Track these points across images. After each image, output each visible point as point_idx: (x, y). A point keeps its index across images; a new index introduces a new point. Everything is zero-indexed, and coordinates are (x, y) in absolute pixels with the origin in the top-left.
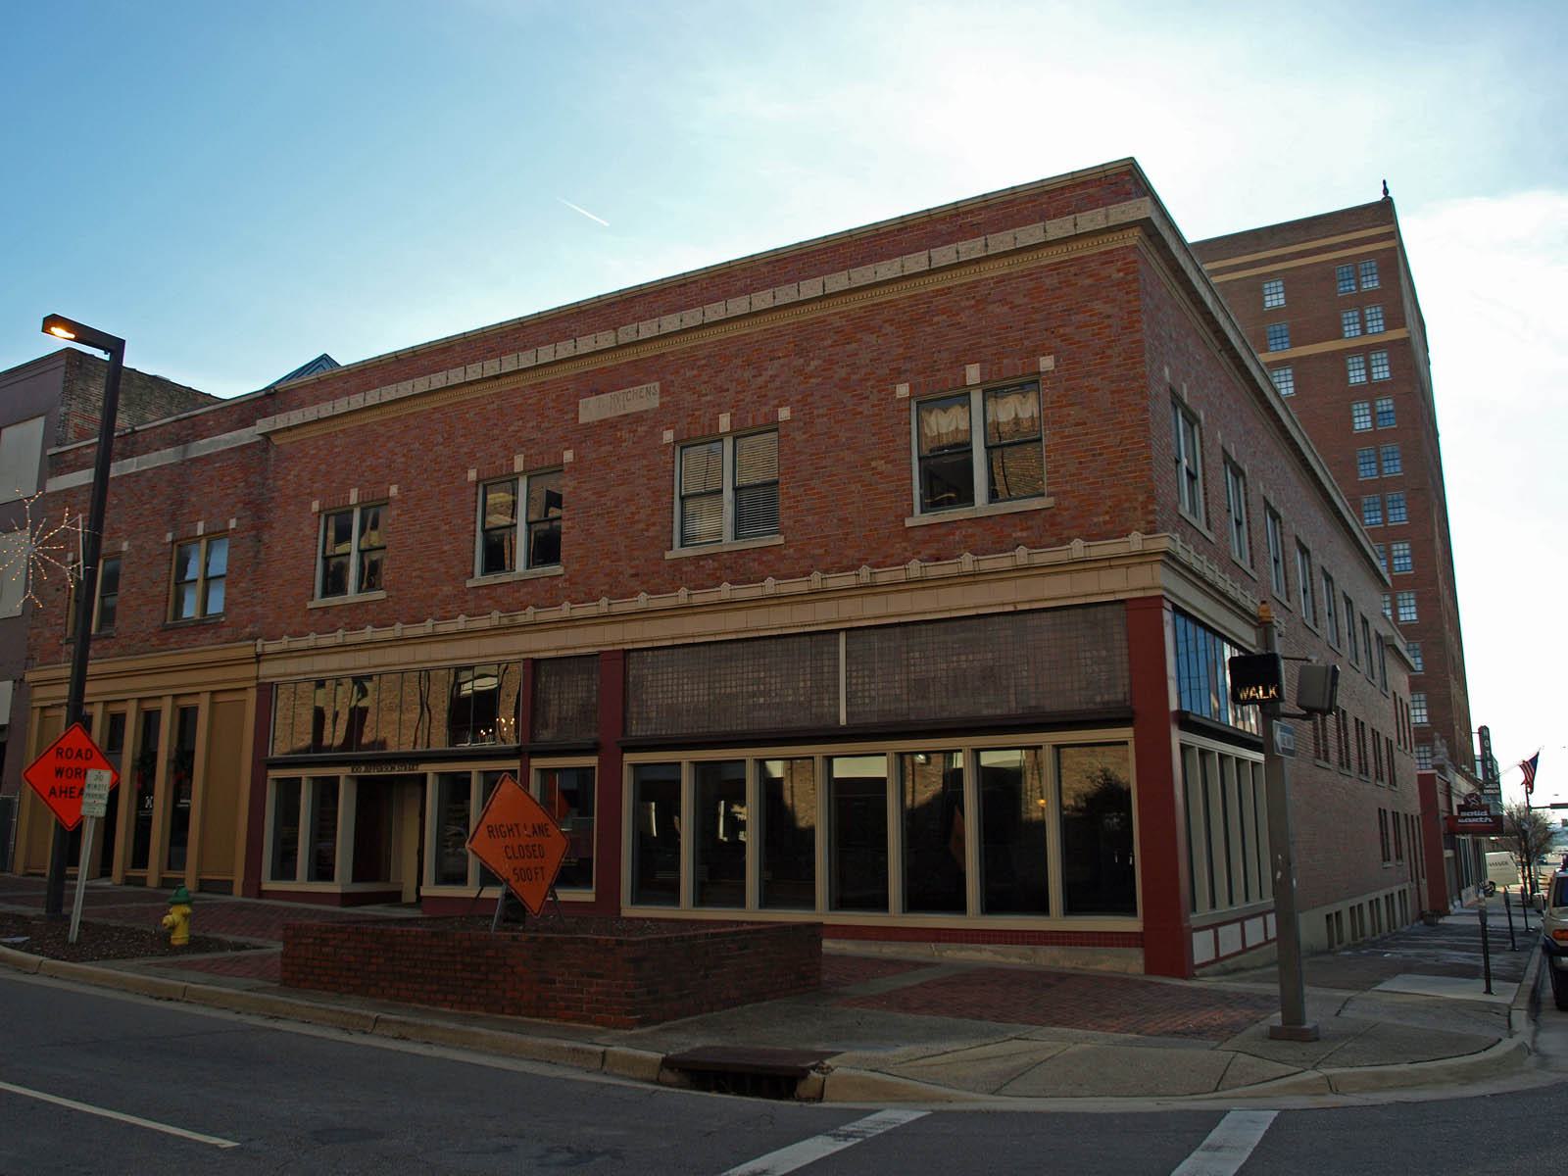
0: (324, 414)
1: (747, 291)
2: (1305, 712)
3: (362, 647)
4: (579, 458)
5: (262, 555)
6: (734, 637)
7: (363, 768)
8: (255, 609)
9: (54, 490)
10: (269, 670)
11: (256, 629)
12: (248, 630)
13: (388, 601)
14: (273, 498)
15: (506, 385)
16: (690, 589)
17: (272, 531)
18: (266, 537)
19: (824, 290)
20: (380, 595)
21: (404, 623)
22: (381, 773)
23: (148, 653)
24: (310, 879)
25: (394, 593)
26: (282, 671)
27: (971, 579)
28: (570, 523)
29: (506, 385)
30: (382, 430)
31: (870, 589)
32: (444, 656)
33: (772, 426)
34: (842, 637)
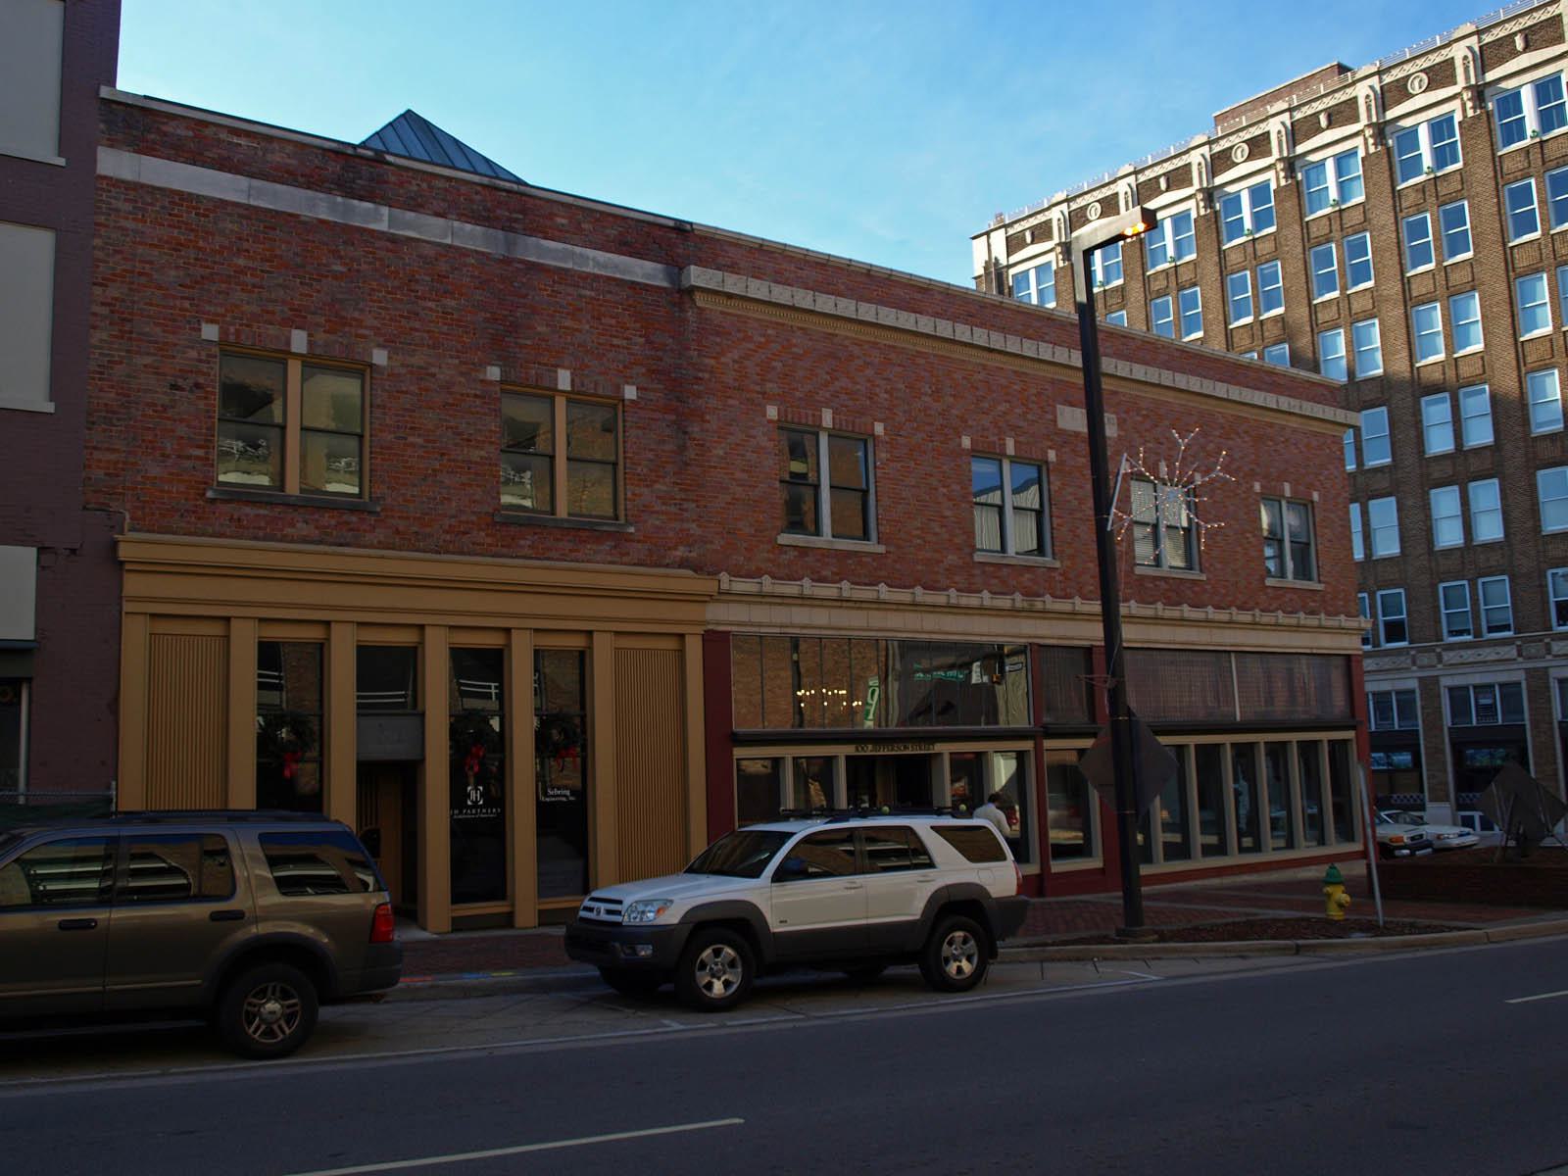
0: (729, 289)
1: (954, 318)
2: (497, 730)
3: (864, 605)
4: (1061, 462)
5: (691, 454)
6: (1139, 645)
7: (870, 747)
8: (686, 526)
9: (1081, 360)
10: (724, 616)
11: (694, 554)
12: (678, 553)
13: (886, 557)
14: (701, 379)
15: (994, 361)
16: (813, 580)
17: (707, 426)
18: (695, 429)
19: (1076, 368)
20: (872, 547)
21: (853, 583)
22: (894, 753)
23: (347, 545)
24: (1165, 843)
25: (892, 549)
26: (745, 619)
27: (932, 609)
28: (1059, 521)
29: (994, 361)
30: (856, 351)
31: (1254, 625)
32: (954, 630)
33: (361, 369)
34: (1233, 655)
